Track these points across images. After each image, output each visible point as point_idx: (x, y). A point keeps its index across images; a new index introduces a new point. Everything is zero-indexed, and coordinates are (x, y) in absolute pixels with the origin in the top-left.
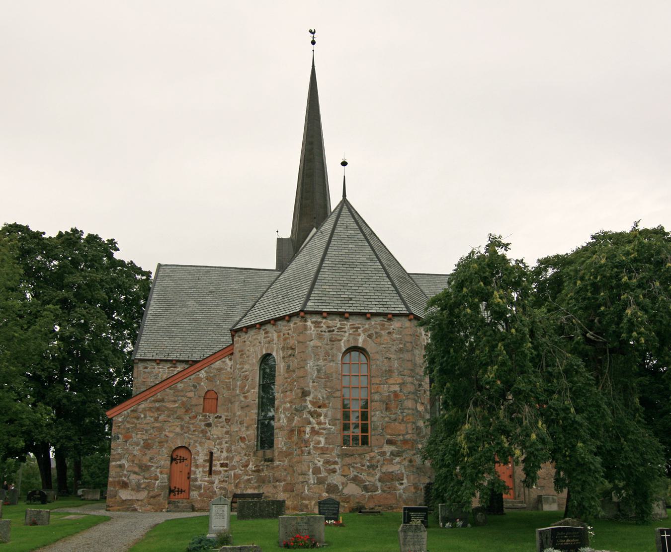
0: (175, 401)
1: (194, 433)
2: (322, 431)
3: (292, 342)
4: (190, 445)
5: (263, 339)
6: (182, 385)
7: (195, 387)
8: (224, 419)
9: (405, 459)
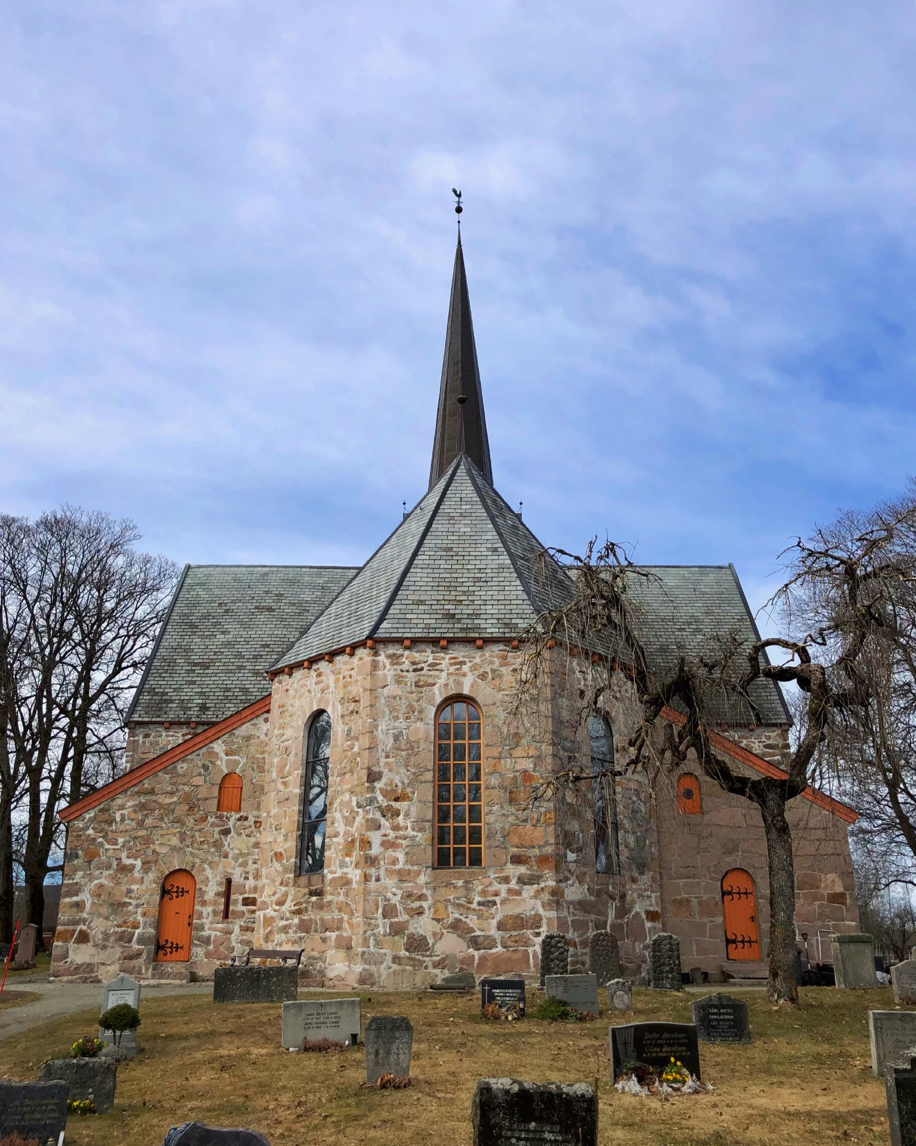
0: (172, 793)
1: (201, 847)
2: (400, 841)
3: (355, 690)
4: (193, 866)
5: (313, 685)
6: (185, 765)
7: (205, 767)
8: (252, 822)
9: (543, 889)
